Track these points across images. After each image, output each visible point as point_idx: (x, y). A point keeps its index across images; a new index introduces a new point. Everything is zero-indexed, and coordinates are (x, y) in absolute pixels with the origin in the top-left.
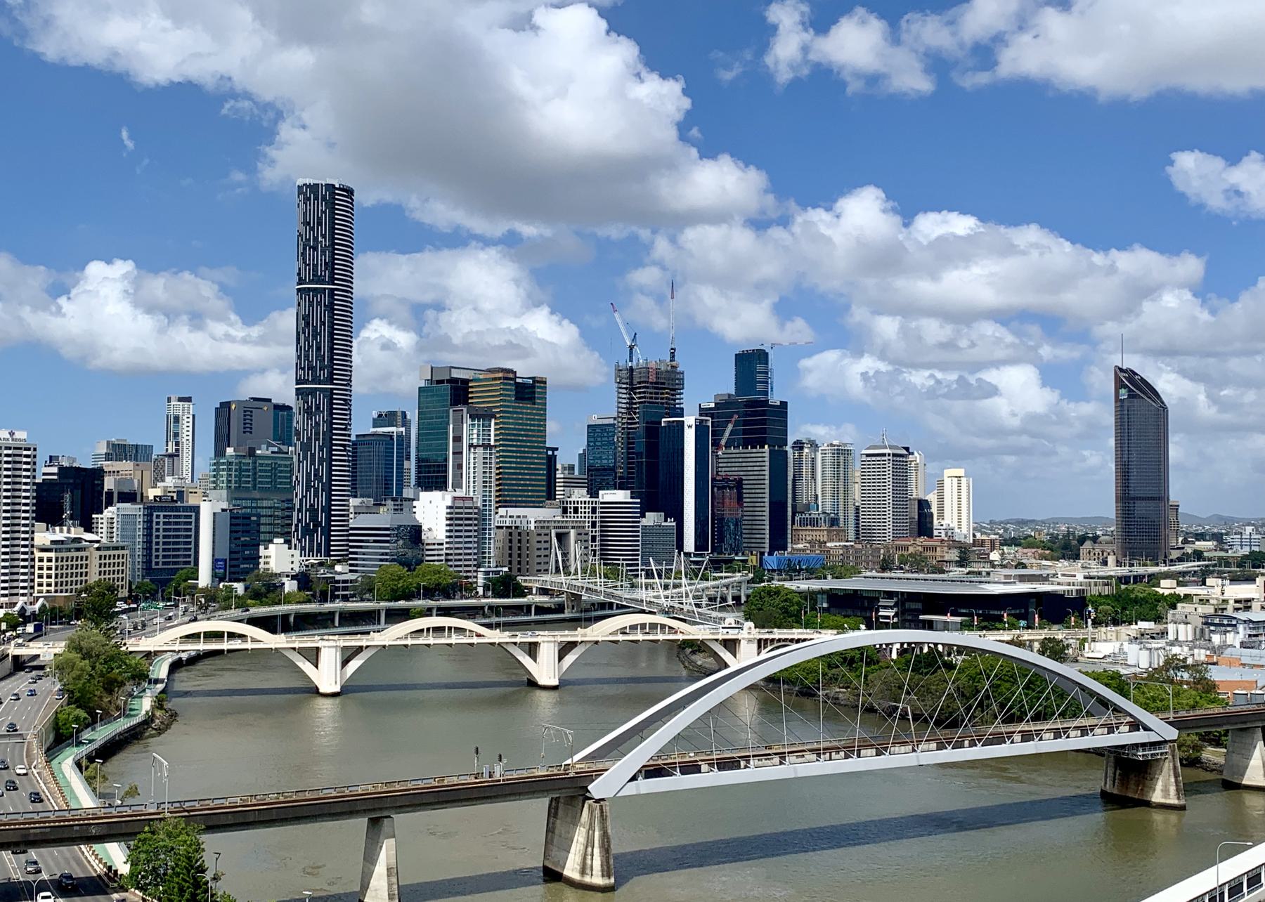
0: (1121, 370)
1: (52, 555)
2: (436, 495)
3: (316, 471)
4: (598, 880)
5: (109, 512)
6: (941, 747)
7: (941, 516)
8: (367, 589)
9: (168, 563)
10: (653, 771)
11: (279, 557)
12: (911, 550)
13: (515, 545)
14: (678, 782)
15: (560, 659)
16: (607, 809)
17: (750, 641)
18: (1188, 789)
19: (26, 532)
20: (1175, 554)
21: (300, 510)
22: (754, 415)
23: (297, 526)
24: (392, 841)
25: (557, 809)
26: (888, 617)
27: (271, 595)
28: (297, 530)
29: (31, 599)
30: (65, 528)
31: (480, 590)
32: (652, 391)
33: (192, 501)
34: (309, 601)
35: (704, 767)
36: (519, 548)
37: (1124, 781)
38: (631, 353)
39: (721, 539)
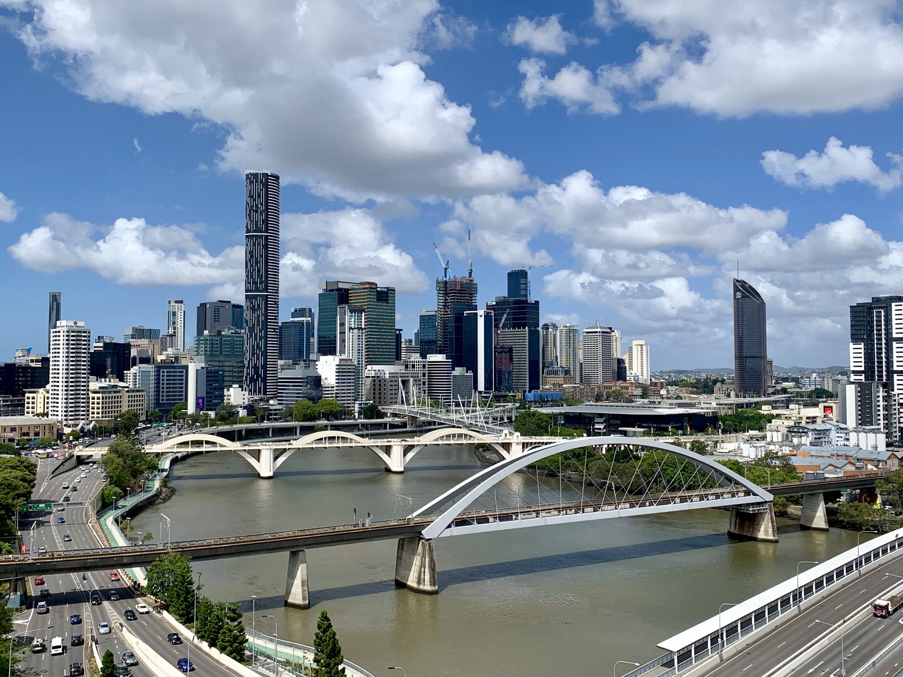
0: (738, 281)
1: (100, 395)
3: (258, 344)
4: (427, 587)
5: (134, 369)
6: (632, 506)
8: (289, 415)
10: (460, 522)
11: (236, 396)
12: (613, 388)
13: (377, 387)
14: (476, 528)
15: (405, 455)
16: (433, 545)
17: (518, 444)
20: (770, 390)
21: (248, 368)
22: (519, 309)
25: (403, 545)
27: (231, 419)
31: (356, 415)
32: (458, 294)
33: (184, 362)
34: (254, 422)
35: (491, 519)
37: (742, 526)
39: (500, 383)
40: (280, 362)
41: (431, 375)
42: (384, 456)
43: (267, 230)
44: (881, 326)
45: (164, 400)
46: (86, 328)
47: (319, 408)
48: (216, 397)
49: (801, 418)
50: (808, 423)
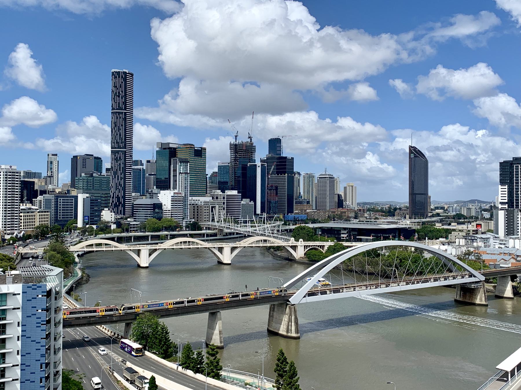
0: (411, 147)
2: (167, 192)
3: (120, 182)
4: (294, 335)
5: (40, 198)
6: (407, 284)
7: (346, 200)
8: (143, 228)
9: (64, 218)
10: (311, 294)
11: (107, 215)
12: (336, 213)
13: (196, 211)
15: (231, 253)
16: (297, 308)
17: (301, 246)
18: (488, 298)
19: (17, 205)
20: (430, 214)
21: (113, 197)
22: (281, 165)
23: (112, 204)
24: (221, 321)
25: (274, 308)
26: (343, 237)
27: (108, 230)
28: (112, 205)
29: (19, 231)
30: (24, 204)
31: (184, 228)
32: (242, 151)
34: (121, 232)
35: (328, 292)
36: (198, 212)
37: (464, 296)
38: (236, 139)
39: (270, 209)
40: (133, 194)
41: (229, 203)
42: (135, 256)
43: (125, 109)
44: (518, 175)
45: (60, 217)
46: (18, 170)
47: (160, 224)
48: (96, 216)
49: (469, 231)
50: (474, 234)
